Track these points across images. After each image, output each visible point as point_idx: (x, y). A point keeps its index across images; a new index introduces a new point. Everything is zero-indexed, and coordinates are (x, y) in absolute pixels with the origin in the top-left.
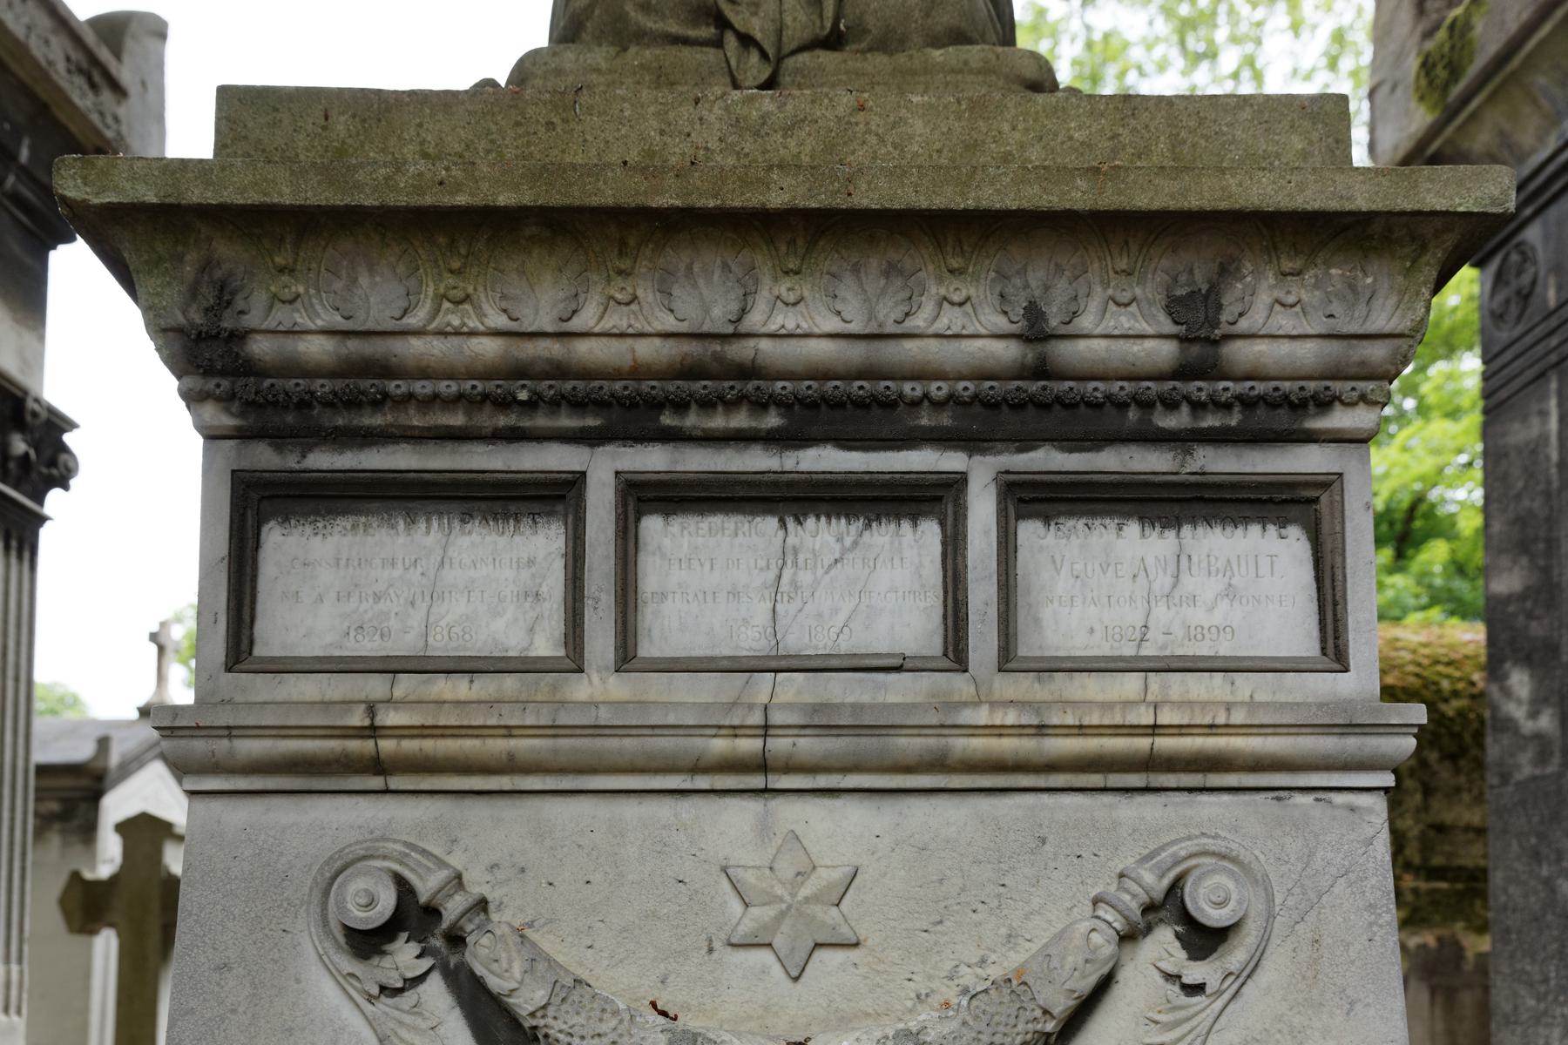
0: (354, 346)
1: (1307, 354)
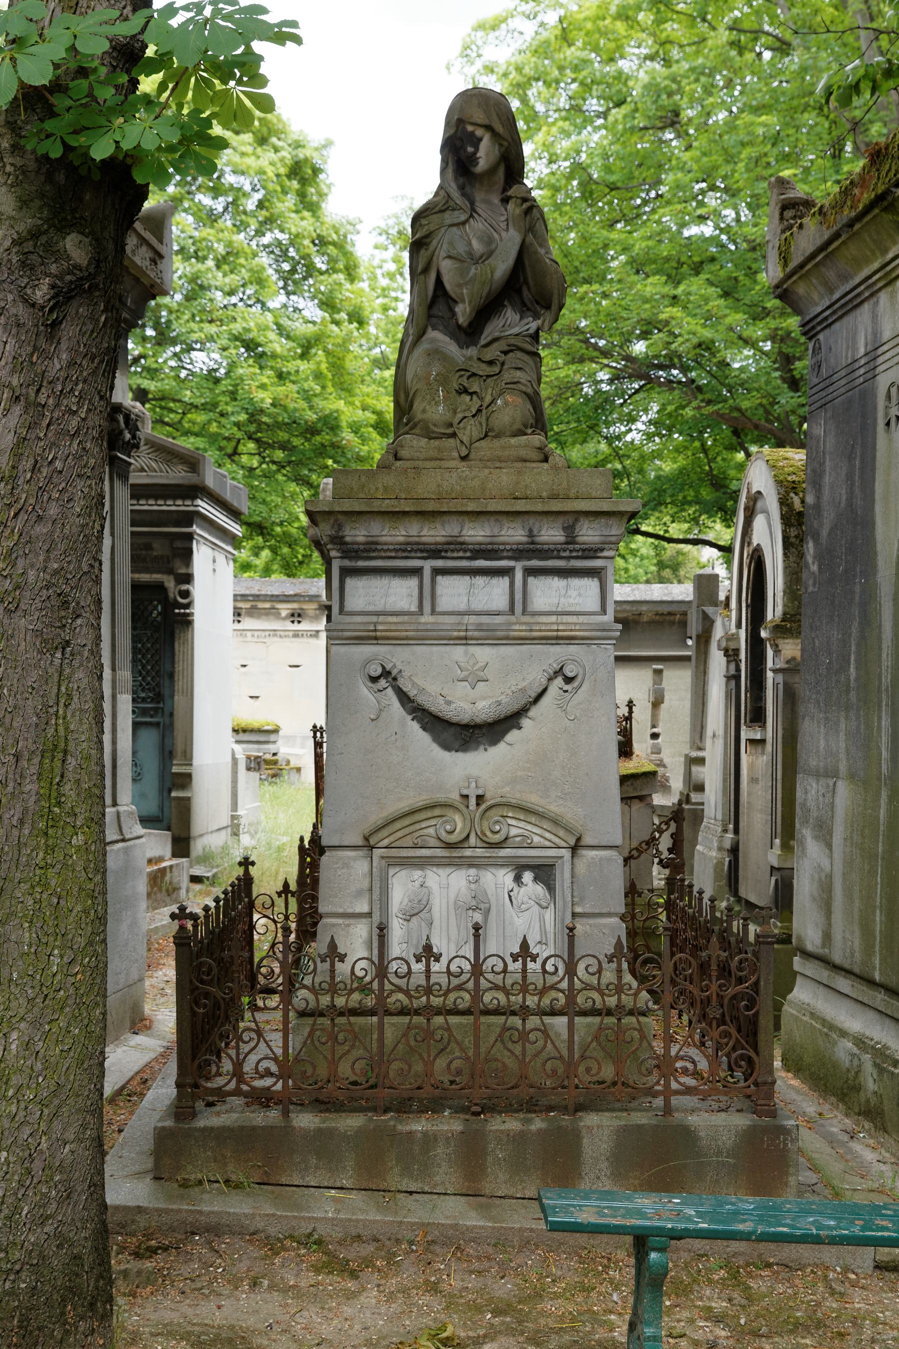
0: (370, 539)
1: (597, 539)
